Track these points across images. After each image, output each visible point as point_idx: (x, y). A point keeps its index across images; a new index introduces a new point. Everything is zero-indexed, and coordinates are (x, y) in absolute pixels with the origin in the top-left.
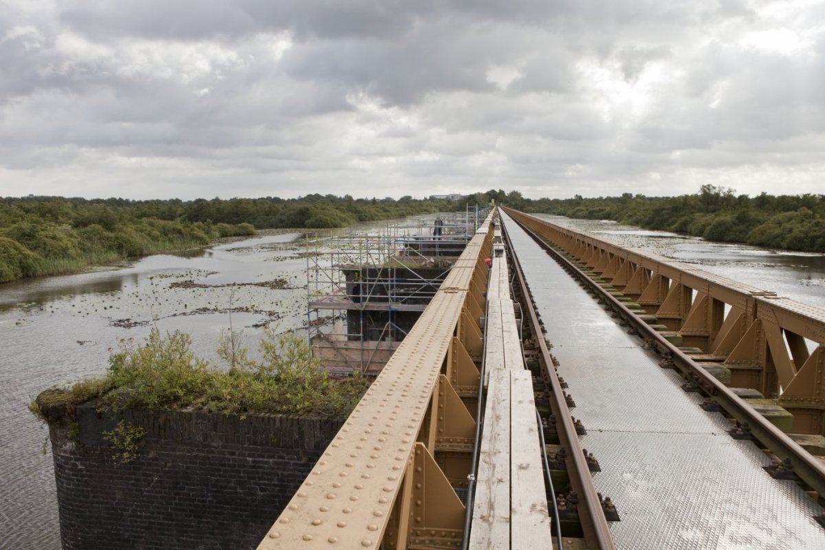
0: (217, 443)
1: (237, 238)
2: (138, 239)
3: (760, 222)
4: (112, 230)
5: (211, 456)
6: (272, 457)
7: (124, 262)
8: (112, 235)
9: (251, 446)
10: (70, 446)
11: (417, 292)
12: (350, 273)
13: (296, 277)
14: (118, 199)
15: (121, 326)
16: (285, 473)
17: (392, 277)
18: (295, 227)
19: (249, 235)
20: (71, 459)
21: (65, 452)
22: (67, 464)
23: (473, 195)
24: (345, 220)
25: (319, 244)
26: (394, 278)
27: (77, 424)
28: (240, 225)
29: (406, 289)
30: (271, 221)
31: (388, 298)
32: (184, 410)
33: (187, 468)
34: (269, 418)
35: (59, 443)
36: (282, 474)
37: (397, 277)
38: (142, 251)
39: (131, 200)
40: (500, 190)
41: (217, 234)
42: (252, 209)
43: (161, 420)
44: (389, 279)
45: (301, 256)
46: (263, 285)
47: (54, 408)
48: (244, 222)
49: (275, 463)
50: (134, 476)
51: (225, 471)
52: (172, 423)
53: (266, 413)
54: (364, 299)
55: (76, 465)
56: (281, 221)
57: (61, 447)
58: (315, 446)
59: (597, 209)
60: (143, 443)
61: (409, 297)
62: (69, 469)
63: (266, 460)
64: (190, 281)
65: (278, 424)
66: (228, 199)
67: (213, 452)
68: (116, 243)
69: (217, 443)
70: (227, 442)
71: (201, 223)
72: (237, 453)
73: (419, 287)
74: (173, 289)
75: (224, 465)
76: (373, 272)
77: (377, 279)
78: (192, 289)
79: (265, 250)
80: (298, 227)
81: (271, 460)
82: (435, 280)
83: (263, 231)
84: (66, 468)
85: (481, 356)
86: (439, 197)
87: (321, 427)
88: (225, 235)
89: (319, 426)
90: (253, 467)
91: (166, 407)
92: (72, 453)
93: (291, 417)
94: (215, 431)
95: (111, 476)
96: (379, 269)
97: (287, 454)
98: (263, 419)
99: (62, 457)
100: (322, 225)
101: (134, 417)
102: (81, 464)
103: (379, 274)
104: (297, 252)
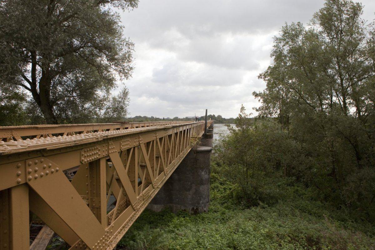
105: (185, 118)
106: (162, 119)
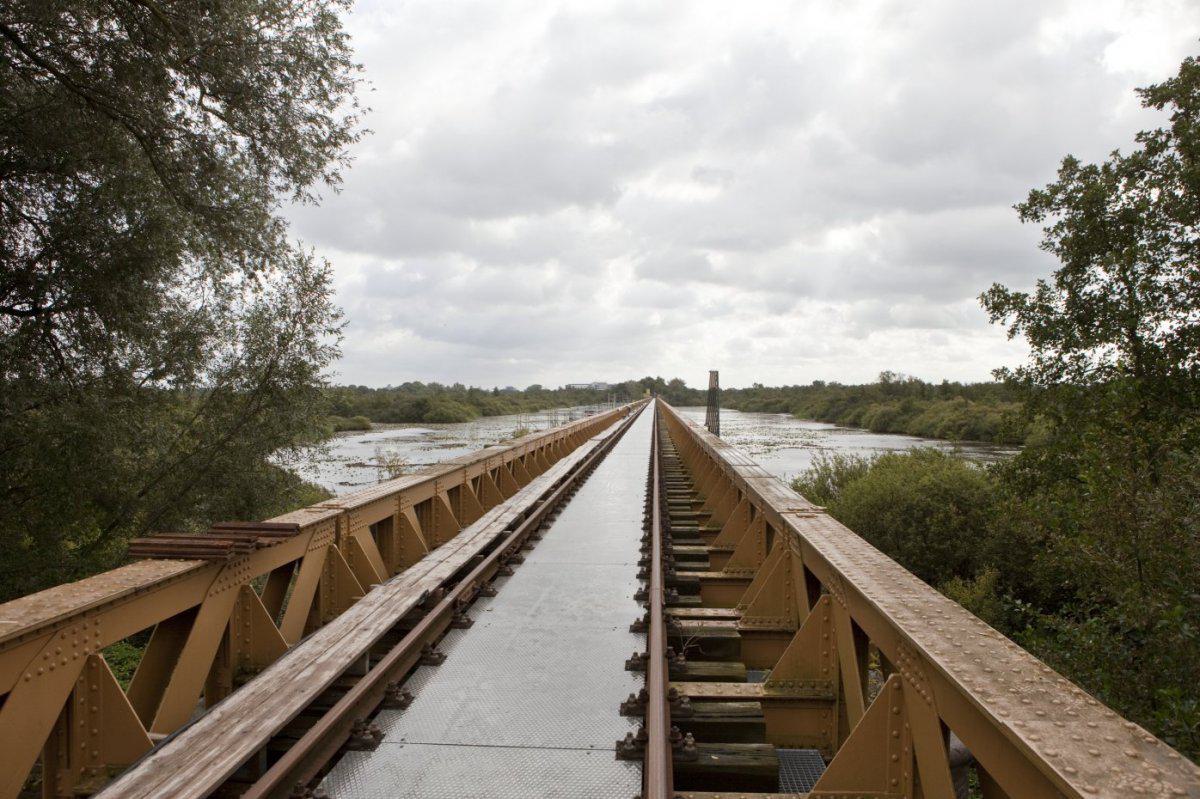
3: (922, 411)
19: (365, 429)
24: (469, 414)
30: (381, 415)
56: (394, 415)
59: (773, 400)
85: (713, 462)
86: (580, 387)
100: (443, 419)
105: (564, 387)
106: (492, 390)
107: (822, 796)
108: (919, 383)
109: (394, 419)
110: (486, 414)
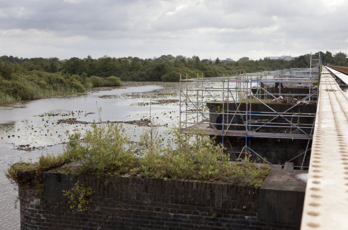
0: (147, 201)
1: (107, 88)
2: (30, 87)
4: (10, 79)
5: (142, 211)
6: (190, 213)
7: (18, 105)
8: (10, 82)
9: (173, 204)
10: (36, 201)
11: (268, 123)
12: (212, 106)
13: (157, 118)
14: (9, 56)
15: (23, 149)
16: (198, 225)
17: (248, 110)
18: (153, 81)
19: (116, 85)
20: (36, 212)
21: (32, 206)
22: (32, 215)
23: (302, 56)
25: (175, 94)
26: (250, 111)
27: (43, 185)
28: (109, 77)
29: (259, 120)
30: (134, 75)
31: (244, 127)
32: (123, 176)
33: (123, 220)
34: (188, 182)
35: (28, 200)
36: (196, 226)
37: (252, 110)
38: (32, 96)
39: (19, 58)
40: (327, 52)
41: (91, 85)
42: (118, 66)
43: (106, 182)
44: (247, 112)
45: (160, 102)
46: (131, 123)
47: (27, 173)
48: (112, 75)
49: (191, 218)
50: (82, 226)
51: (152, 223)
52: (114, 185)
53: (186, 179)
54: (225, 127)
55: (40, 217)
56: (142, 76)
57: (30, 203)
58: (223, 205)
60: (91, 200)
61: (263, 126)
62: (35, 220)
63: (183, 215)
64: (73, 119)
65: (195, 187)
66: (97, 59)
67: (144, 208)
68: (12, 89)
69: (147, 201)
70: (155, 201)
71: (78, 75)
72: (162, 209)
73: (269, 118)
74: (60, 124)
75: (152, 218)
76: (232, 106)
77: (236, 111)
78: (75, 125)
79: (130, 97)
80: (156, 81)
81: (188, 215)
82: (284, 113)
83: (127, 83)
84: (31, 219)
87: (228, 190)
88: (97, 86)
89: (226, 190)
90: (174, 220)
91: (109, 174)
92: (37, 207)
93: (205, 182)
94: (147, 192)
95: (65, 225)
96: (238, 104)
97: (201, 211)
98: (183, 183)
99: (29, 210)
100: (174, 79)
101: (85, 181)
102: (44, 216)
103: (238, 108)
104: (156, 99)
105: (263, 59)
107: (170, 229)
108: (42, 58)
109: (141, 79)
110: (207, 76)
